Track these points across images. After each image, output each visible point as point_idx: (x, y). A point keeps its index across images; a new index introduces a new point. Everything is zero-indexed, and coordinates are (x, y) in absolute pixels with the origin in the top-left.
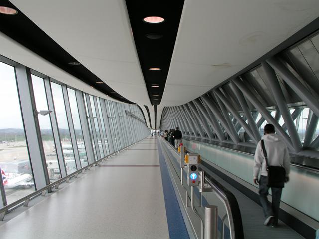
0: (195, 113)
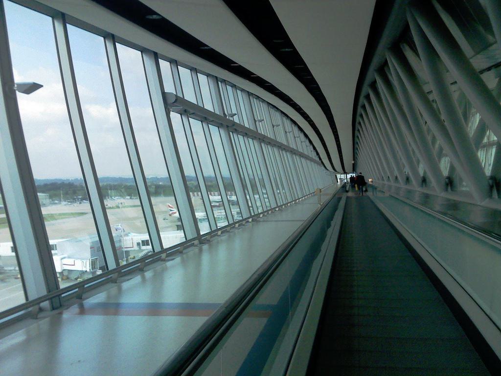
0: (383, 119)
